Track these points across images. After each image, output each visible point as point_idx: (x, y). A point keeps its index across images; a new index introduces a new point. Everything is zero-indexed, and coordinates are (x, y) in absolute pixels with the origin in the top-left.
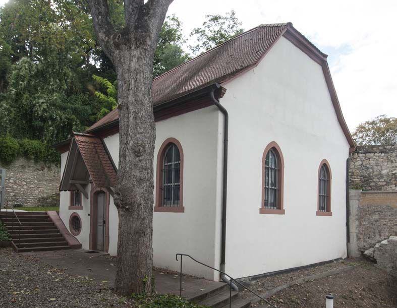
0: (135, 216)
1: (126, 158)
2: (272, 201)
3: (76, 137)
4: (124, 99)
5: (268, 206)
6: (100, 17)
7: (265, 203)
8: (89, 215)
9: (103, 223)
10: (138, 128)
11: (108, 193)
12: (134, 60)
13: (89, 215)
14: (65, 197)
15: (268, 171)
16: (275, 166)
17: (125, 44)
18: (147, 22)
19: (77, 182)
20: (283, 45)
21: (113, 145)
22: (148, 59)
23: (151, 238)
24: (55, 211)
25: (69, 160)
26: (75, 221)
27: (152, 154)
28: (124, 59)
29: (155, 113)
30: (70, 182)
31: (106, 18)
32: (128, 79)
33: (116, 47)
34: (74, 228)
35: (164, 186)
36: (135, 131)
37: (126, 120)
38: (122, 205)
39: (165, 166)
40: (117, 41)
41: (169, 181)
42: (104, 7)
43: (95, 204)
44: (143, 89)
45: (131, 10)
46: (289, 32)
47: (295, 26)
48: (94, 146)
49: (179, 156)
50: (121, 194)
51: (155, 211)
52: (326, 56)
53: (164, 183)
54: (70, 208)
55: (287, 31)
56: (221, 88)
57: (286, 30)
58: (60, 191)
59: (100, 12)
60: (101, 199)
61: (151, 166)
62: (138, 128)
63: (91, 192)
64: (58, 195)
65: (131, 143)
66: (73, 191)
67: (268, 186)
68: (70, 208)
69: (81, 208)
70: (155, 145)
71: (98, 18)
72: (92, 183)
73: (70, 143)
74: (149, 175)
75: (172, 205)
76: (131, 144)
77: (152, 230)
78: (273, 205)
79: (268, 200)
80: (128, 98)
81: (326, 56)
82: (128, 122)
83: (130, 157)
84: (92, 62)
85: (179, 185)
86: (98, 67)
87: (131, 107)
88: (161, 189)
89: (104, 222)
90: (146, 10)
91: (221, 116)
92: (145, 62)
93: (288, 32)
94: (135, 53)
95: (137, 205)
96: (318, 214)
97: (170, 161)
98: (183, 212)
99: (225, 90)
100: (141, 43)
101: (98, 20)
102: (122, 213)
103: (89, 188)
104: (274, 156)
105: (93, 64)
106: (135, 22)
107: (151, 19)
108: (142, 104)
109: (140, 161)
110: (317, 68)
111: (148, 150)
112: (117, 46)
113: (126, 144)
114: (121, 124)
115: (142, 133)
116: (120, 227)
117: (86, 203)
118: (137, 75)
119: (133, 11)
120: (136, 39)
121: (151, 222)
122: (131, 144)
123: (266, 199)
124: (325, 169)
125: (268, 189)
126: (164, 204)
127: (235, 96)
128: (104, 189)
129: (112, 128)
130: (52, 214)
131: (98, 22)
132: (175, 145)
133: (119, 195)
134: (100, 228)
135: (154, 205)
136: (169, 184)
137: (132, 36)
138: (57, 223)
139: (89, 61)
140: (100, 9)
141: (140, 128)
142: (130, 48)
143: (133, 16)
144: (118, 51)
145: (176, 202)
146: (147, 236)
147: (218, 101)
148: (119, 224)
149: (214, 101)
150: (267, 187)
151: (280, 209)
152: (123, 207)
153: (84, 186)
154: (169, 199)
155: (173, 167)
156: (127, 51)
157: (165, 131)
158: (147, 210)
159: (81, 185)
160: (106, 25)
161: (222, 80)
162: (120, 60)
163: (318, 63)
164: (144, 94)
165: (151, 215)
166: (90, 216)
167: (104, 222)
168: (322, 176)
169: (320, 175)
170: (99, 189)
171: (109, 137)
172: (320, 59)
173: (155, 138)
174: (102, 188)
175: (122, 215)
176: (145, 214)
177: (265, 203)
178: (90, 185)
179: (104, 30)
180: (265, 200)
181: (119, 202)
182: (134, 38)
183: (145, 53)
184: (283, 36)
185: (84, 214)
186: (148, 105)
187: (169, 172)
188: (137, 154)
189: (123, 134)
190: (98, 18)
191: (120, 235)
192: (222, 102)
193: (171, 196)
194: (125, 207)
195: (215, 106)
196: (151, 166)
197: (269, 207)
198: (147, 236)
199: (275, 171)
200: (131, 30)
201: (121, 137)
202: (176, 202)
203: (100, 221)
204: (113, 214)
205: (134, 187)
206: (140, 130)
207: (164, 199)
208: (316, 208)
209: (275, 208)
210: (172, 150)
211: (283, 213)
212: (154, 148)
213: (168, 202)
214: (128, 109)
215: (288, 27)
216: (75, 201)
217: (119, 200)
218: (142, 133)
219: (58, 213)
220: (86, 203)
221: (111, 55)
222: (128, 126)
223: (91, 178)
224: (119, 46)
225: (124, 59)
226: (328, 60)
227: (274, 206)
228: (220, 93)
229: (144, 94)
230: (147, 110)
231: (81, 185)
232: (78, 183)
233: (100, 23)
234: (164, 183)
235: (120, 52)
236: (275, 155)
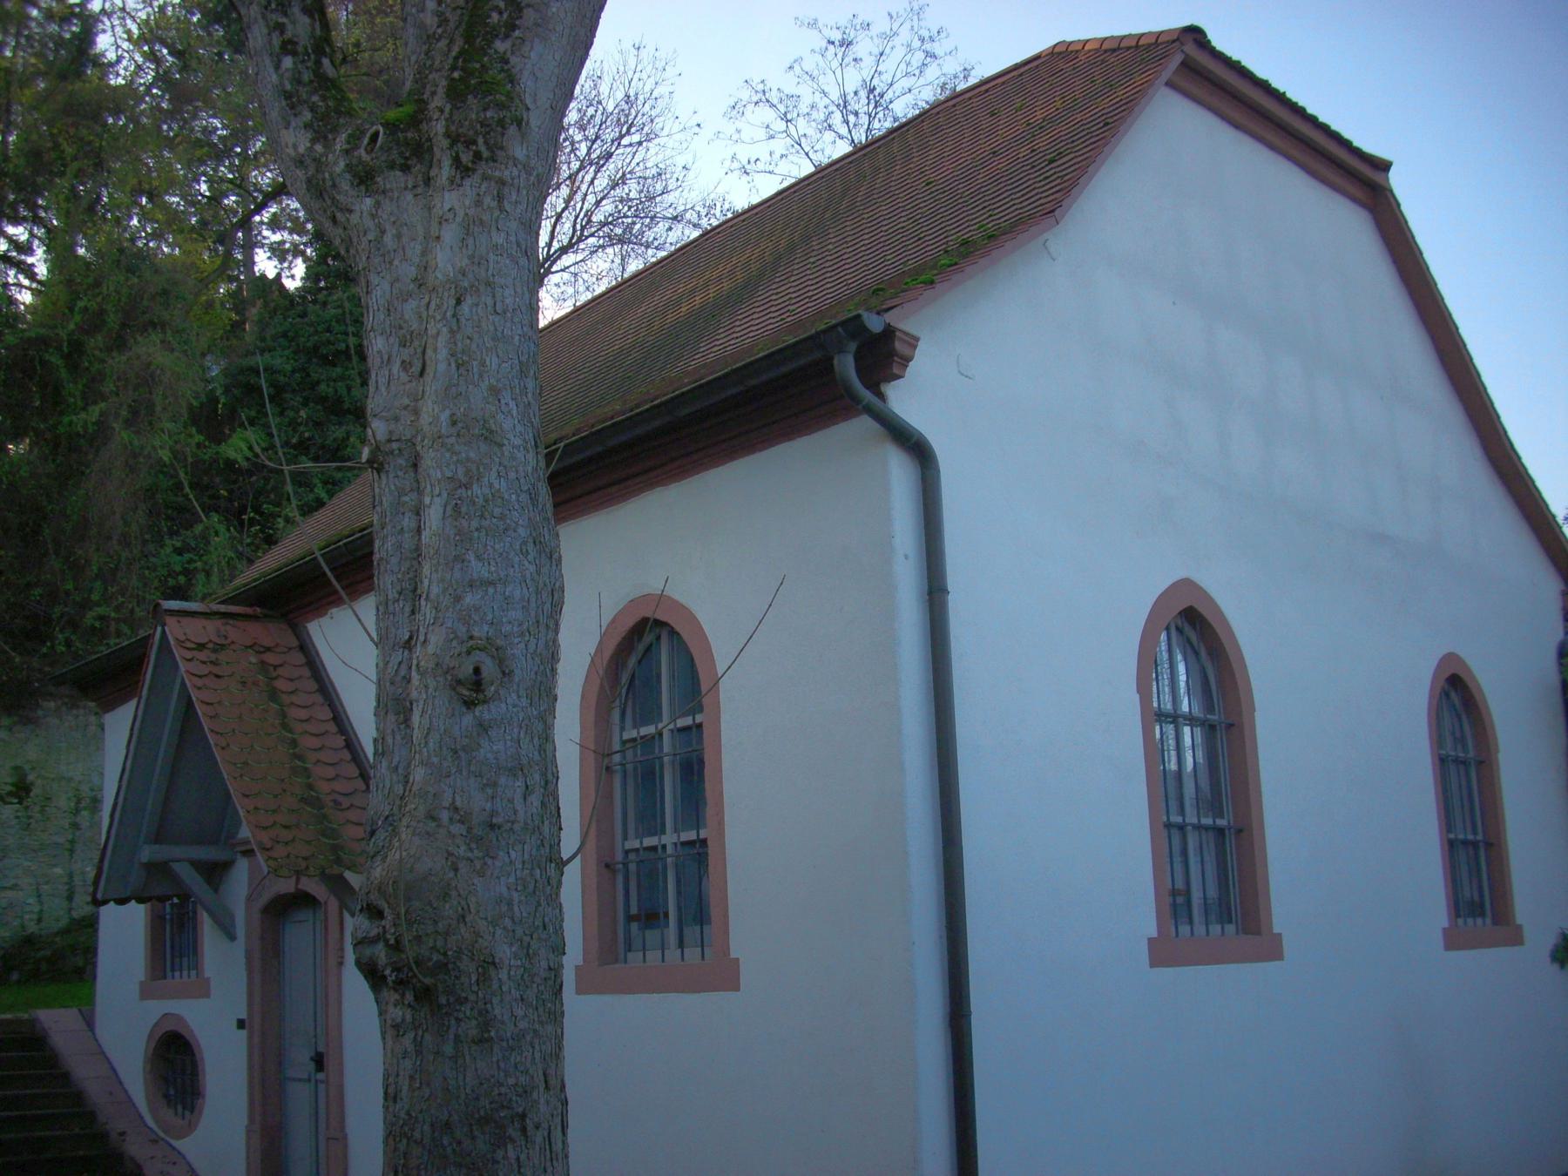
0: (471, 1029)
1: (407, 721)
2: (1212, 892)
3: (171, 621)
4: (397, 419)
5: (1191, 922)
6: (288, 62)
7: (1175, 903)
8: (241, 1024)
9: (312, 1066)
10: (471, 556)
11: (333, 904)
12: (450, 234)
13: (241, 1024)
14: (124, 931)
15: (1467, 774)
16: (1209, 706)
17: (405, 169)
18: (507, 62)
19: (178, 851)
20: (1173, 128)
21: (347, 644)
22: (514, 225)
23: (558, 1146)
24: (75, 1010)
25: (140, 743)
26: (175, 1056)
27: (544, 692)
28: (399, 236)
29: (555, 481)
30: (147, 853)
31: (318, 63)
32: (415, 326)
33: (361, 182)
34: (166, 1096)
35: (627, 852)
36: (457, 574)
37: (408, 522)
38: (397, 969)
39: (624, 743)
40: (365, 157)
41: (651, 820)
42: (307, 20)
43: (268, 962)
44: (492, 361)
45: (430, 20)
46: (1193, 66)
47: (1219, 41)
48: (263, 662)
49: (695, 688)
50: (387, 912)
51: (580, 990)
52: (1384, 166)
53: (625, 838)
54: (146, 993)
55: (1183, 63)
56: (889, 333)
57: (1177, 60)
58: (98, 903)
59: (291, 42)
60: (299, 934)
61: (541, 750)
62: (471, 556)
63: (249, 899)
64: (91, 924)
65: (433, 639)
66: (162, 899)
67: (1182, 811)
68: (146, 993)
69: (203, 990)
70: (564, 638)
71: (277, 67)
72: (249, 853)
73: (141, 660)
74: (535, 800)
75: (673, 954)
76: (436, 639)
77: (565, 1102)
78: (1223, 911)
79: (1188, 892)
80: (416, 412)
81: (1384, 166)
82: (419, 531)
83: (432, 709)
84: (265, 265)
85: (704, 842)
86: (291, 285)
87: (429, 459)
88: (607, 866)
89: (319, 1061)
90: (501, 13)
91: (899, 471)
92: (499, 239)
93: (1188, 66)
94: (453, 200)
95: (472, 968)
96: (1453, 940)
97: (649, 713)
98: (737, 989)
99: (913, 342)
100: (478, 156)
101: (281, 76)
102: (396, 1013)
103: (240, 879)
104: (1196, 653)
105: (271, 274)
106: (453, 68)
107: (526, 48)
108: (490, 437)
109: (483, 727)
110: (1342, 223)
111: (523, 668)
112: (365, 178)
113: (408, 645)
114: (384, 548)
115: (491, 583)
116: (391, 1097)
117: (224, 960)
118: (459, 302)
119: (443, 21)
120: (454, 139)
121: (557, 1054)
122: (436, 639)
123: (1180, 885)
124: (1456, 694)
125: (1181, 828)
126: (629, 948)
127: (967, 368)
128: (312, 886)
129: (348, 569)
130: (58, 1022)
131: (282, 84)
132: (673, 633)
133: (380, 914)
134: (299, 1097)
135: (574, 956)
136: (649, 841)
137: (439, 127)
138: (84, 1073)
139: (254, 263)
140: (289, 27)
141: (478, 558)
142: (428, 181)
143: (443, 44)
144: (368, 201)
145: (692, 932)
146: (539, 1137)
147: (881, 396)
148: (386, 1076)
149: (855, 399)
150: (1177, 819)
151: (1258, 933)
152: (400, 984)
153: (215, 872)
154: (651, 917)
155: (667, 748)
156: (410, 197)
157: (615, 561)
158: (531, 995)
159: (197, 865)
160: (315, 91)
161: (896, 296)
162: (379, 240)
163: (1354, 200)
164: (495, 391)
165: (556, 1017)
166: (243, 1033)
167: (319, 1061)
168: (1449, 742)
169: (1437, 739)
170: (286, 886)
171: (334, 610)
172: (1360, 178)
173: (557, 607)
174: (304, 880)
175: (396, 1027)
176: (519, 1012)
177: (1174, 905)
178: (242, 865)
179: (308, 116)
180: (1174, 893)
181: (380, 953)
182: (447, 135)
183: (500, 198)
184: (1170, 84)
185: (217, 1020)
186: (518, 442)
187: (649, 777)
188: (472, 690)
189: (392, 594)
190: (277, 67)
191: (396, 1134)
192: (907, 399)
193: (666, 900)
194: (421, 984)
195: (864, 423)
196: (541, 750)
197: (1200, 929)
198: (539, 1137)
199: (1210, 729)
200: (432, 106)
201: (383, 611)
202: (692, 932)
203: (300, 1058)
204: (361, 1018)
205: (456, 870)
206: (478, 569)
207: (630, 918)
208: (1438, 914)
209: (1230, 928)
210: (653, 656)
211: (1272, 950)
212: (554, 657)
213: (652, 936)
214: (415, 466)
215: (1191, 49)
216: (173, 949)
217: (381, 945)
218: (491, 583)
219: (90, 1023)
220: (224, 960)
221: (334, 220)
222: (418, 554)
223: (245, 832)
224: (372, 178)
225: (399, 236)
226: (1398, 181)
227: (1225, 916)
228: (883, 356)
229: (495, 391)
230: (520, 466)
231: (197, 865)
232: (182, 857)
233: (288, 87)
234: (625, 838)
235: (378, 204)
236: (1203, 653)
